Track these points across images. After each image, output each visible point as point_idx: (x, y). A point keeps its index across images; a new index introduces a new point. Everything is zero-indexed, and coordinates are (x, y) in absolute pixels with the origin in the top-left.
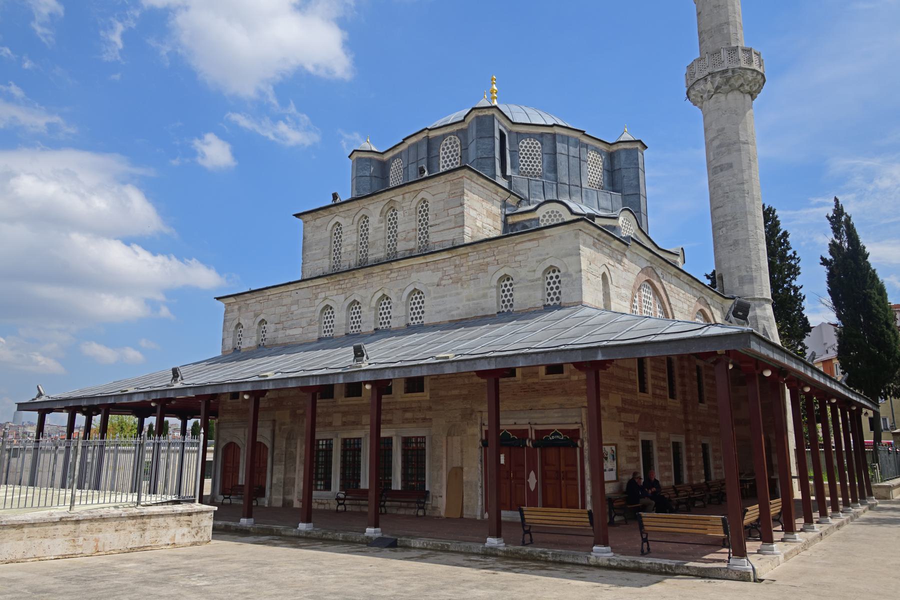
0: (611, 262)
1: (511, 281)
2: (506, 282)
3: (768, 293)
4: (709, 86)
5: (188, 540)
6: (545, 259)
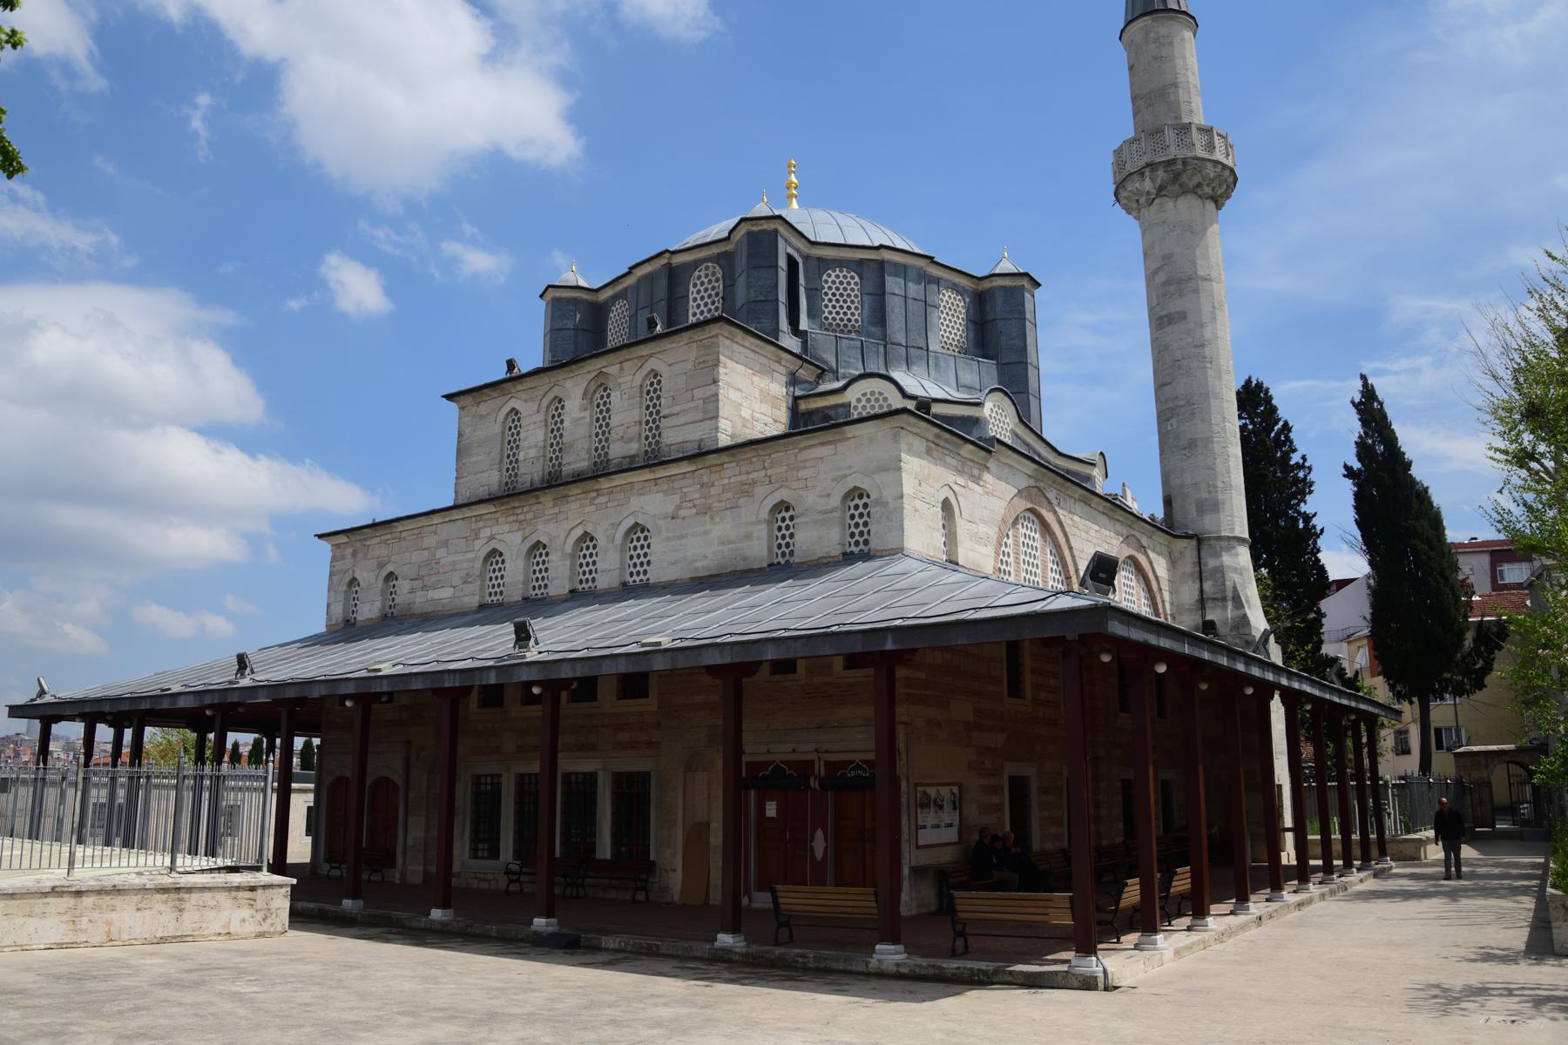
0: (961, 481)
1: (791, 512)
2: (857, 501)
3: (1242, 529)
4: (1148, 185)
5: (251, 928)
6: (845, 476)
